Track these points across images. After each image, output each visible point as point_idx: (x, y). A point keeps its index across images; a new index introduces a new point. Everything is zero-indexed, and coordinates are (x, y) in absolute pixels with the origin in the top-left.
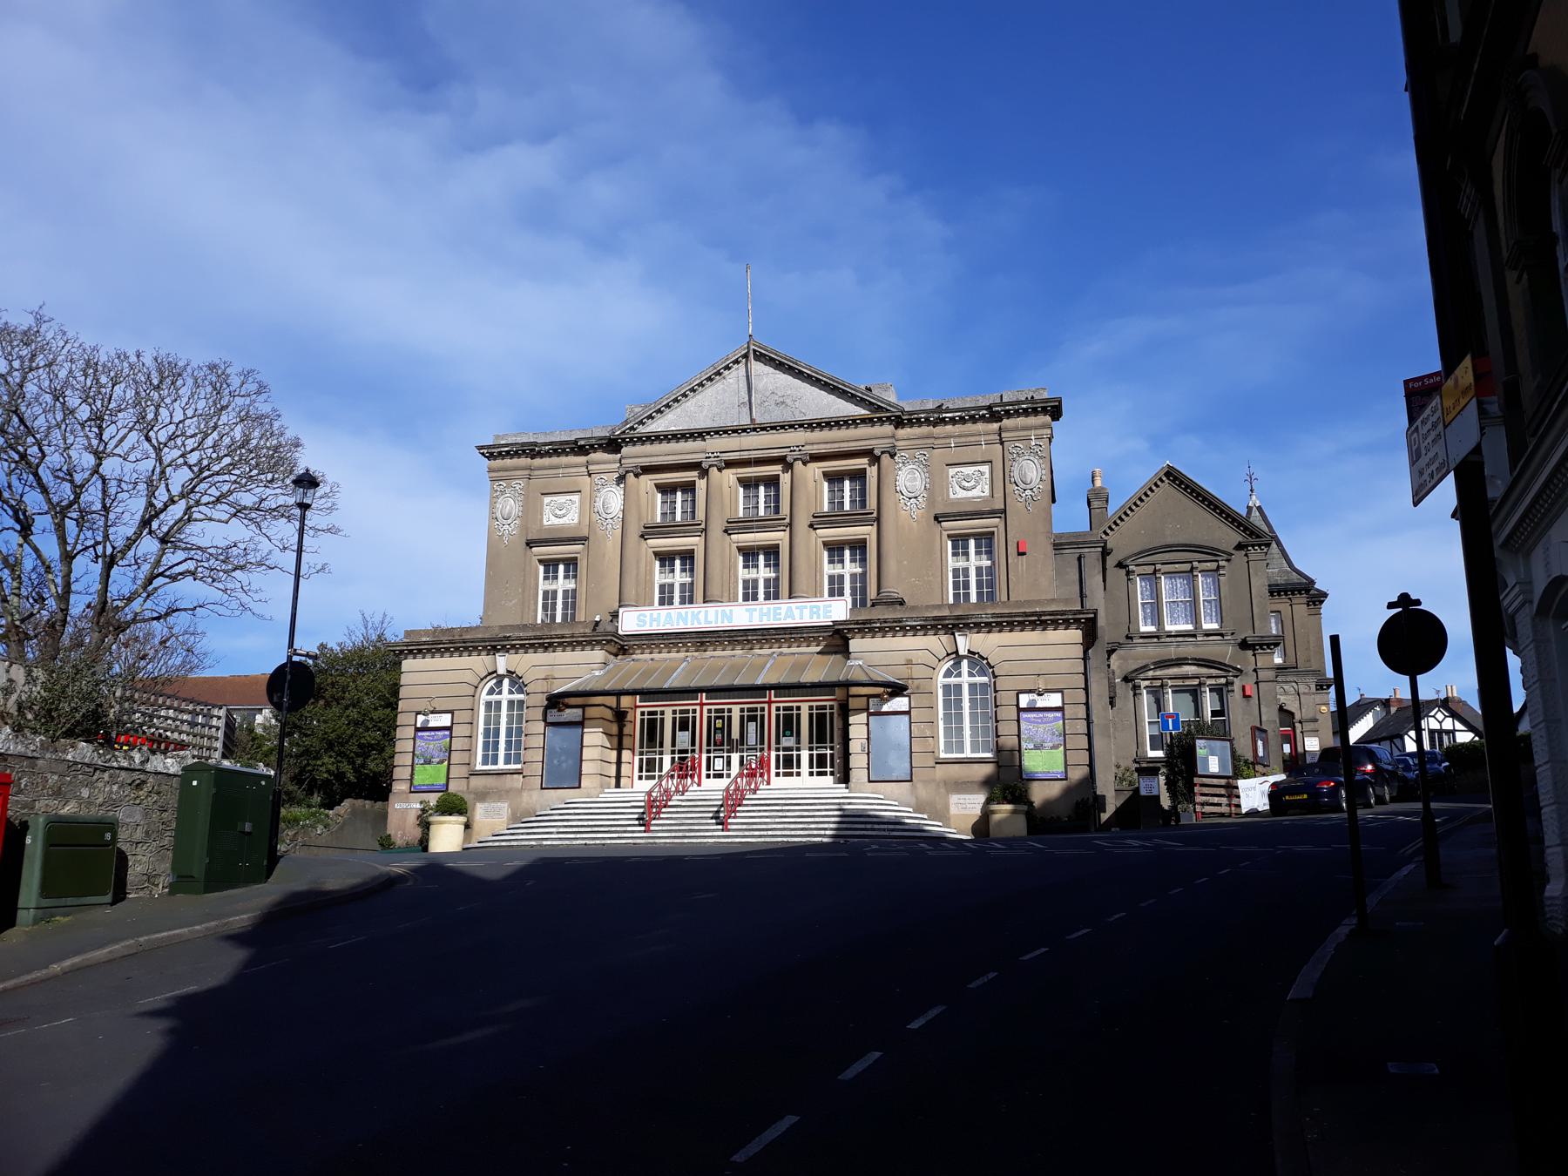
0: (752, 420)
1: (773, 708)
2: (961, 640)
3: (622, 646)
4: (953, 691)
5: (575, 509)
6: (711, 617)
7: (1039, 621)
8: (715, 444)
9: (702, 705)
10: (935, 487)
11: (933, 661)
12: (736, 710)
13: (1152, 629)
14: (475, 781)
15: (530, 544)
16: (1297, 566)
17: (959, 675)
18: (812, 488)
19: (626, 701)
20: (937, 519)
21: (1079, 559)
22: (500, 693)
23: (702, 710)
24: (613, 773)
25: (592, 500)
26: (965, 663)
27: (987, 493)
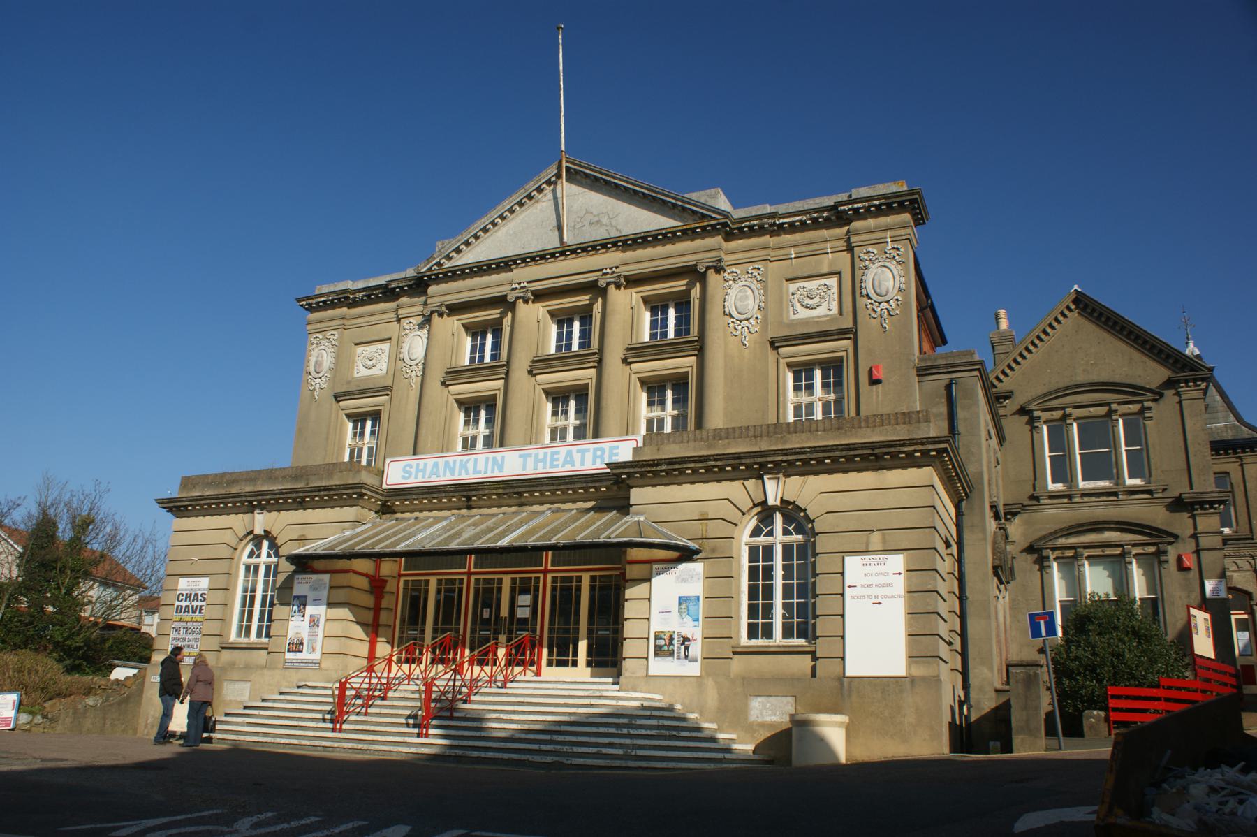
0: (1193, 517)
1: (548, 575)
2: (770, 485)
3: (391, 503)
4: (761, 555)
5: (384, 359)
6: (481, 467)
7: (877, 457)
8: (522, 274)
9: (470, 574)
10: (771, 305)
11: (733, 514)
12: (507, 580)
13: (1060, 486)
14: (227, 656)
15: (338, 397)
16: (1247, 419)
17: (770, 533)
18: (628, 315)
19: (387, 568)
20: (774, 344)
21: (948, 387)
22: (259, 556)
23: (470, 578)
24: (365, 653)
25: (399, 347)
26: (778, 518)
27: (835, 310)
